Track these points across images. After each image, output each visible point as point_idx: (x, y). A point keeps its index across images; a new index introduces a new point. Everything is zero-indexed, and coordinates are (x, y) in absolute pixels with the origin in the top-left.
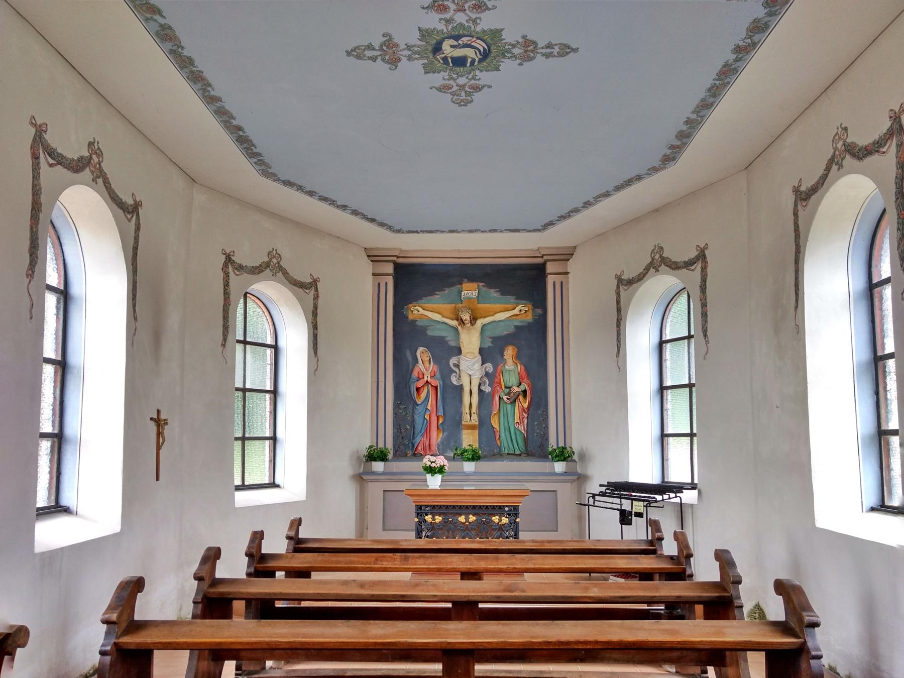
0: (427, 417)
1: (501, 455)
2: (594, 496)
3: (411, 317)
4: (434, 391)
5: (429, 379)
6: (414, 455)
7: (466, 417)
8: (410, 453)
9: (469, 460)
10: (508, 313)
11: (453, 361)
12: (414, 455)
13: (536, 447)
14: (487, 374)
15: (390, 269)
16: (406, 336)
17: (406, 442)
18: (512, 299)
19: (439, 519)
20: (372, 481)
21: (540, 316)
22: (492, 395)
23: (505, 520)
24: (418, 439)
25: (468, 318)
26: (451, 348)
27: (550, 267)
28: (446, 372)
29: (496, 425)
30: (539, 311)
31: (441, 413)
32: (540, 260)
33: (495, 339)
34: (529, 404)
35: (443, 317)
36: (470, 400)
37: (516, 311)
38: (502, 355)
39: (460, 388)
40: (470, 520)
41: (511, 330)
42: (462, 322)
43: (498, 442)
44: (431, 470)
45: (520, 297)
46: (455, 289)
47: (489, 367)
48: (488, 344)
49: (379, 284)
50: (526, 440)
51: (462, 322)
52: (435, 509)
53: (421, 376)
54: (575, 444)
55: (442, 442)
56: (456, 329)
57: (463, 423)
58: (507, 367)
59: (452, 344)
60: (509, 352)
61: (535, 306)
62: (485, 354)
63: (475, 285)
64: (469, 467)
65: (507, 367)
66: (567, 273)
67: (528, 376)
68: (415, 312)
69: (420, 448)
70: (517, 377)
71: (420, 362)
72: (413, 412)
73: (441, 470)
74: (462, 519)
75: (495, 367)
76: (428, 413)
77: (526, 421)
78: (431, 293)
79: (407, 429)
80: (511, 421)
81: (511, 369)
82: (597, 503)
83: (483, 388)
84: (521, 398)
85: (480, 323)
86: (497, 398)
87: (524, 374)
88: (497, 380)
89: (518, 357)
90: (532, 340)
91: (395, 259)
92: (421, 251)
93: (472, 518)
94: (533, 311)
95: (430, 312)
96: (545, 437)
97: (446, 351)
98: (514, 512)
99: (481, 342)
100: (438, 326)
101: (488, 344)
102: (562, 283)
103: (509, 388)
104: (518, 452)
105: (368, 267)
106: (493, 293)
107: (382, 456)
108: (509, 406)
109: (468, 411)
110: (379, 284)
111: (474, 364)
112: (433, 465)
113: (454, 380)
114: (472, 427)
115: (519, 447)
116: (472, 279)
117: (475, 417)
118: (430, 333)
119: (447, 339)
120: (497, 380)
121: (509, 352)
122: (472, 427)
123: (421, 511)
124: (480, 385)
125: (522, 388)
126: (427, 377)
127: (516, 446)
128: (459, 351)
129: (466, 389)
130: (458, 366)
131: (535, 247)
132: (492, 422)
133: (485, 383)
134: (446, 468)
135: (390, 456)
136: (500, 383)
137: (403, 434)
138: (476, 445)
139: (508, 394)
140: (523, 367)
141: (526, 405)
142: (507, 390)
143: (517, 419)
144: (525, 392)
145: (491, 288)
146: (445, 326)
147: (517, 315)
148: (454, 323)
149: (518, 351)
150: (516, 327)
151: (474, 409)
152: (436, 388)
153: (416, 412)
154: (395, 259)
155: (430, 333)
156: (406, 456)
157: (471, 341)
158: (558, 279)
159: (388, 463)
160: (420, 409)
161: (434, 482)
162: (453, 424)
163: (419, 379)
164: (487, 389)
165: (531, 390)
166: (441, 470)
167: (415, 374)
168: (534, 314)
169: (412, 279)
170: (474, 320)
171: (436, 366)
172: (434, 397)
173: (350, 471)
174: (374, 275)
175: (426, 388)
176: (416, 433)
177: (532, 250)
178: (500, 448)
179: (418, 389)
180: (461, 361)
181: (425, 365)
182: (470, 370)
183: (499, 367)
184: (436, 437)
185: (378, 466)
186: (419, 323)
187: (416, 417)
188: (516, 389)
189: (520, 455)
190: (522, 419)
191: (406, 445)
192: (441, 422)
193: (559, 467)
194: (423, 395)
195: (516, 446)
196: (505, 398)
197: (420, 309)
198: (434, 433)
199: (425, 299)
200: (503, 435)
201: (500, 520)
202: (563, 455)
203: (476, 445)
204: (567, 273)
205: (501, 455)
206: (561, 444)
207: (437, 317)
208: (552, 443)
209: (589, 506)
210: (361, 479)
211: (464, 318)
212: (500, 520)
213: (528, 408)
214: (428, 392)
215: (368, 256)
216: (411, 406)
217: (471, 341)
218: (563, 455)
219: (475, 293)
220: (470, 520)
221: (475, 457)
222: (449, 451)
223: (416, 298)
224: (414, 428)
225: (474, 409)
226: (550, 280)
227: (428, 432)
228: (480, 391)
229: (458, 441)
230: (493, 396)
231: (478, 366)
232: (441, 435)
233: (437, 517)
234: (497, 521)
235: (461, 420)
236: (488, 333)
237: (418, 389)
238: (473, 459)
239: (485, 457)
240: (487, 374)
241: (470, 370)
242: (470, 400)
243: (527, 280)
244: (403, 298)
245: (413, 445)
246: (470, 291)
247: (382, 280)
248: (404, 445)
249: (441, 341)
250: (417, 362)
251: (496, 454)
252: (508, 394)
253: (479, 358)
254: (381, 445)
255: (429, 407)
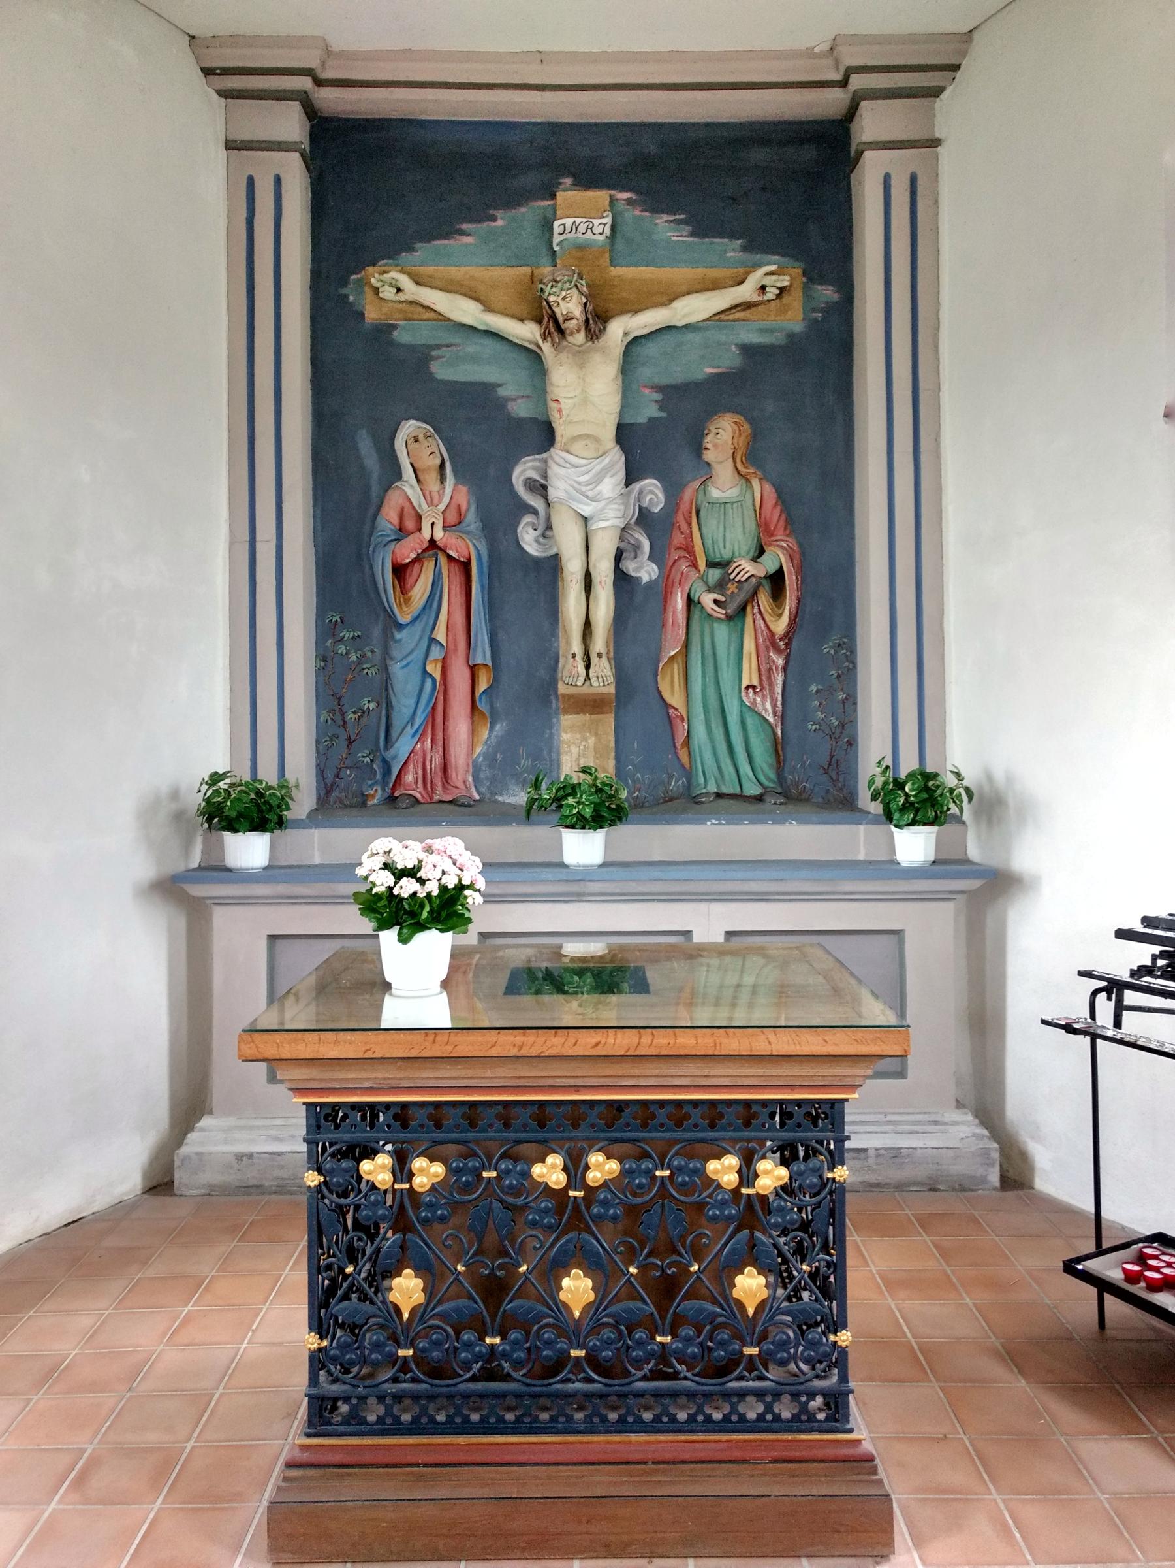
0: (434, 670)
1: (695, 800)
2: (1114, 987)
3: (372, 314)
4: (458, 579)
5: (439, 534)
6: (392, 800)
7: (571, 673)
8: (377, 795)
9: (580, 823)
10: (715, 298)
11: (524, 471)
12: (392, 800)
13: (812, 772)
14: (644, 518)
15: (290, 124)
16: (359, 380)
17: (363, 756)
18: (731, 248)
19: (427, 1173)
20: (223, 902)
21: (829, 309)
22: (663, 589)
23: (771, 1175)
24: (403, 747)
25: (577, 311)
26: (520, 423)
27: (873, 123)
28: (501, 511)
29: (675, 698)
30: (827, 293)
31: (482, 655)
32: (831, 102)
33: (671, 393)
34: (793, 621)
35: (488, 308)
36: (586, 610)
37: (746, 292)
38: (698, 449)
39: (552, 566)
40: (594, 1177)
41: (730, 360)
42: (555, 327)
43: (683, 754)
44: (400, 914)
45: (758, 244)
46: (530, 212)
47: (652, 492)
48: (648, 410)
49: (251, 181)
50: (778, 748)
51: (555, 327)
52: (410, 1127)
53: (410, 524)
54: (961, 756)
55: (491, 759)
56: (534, 356)
57: (562, 689)
58: (715, 493)
59: (521, 409)
60: (724, 435)
61: (812, 277)
62: (640, 449)
63: (601, 196)
64: (583, 848)
65: (715, 493)
66: (934, 143)
67: (791, 523)
68: (388, 293)
69: (409, 778)
70: (751, 525)
71: (408, 473)
72: (386, 653)
73: (447, 909)
74: (550, 1171)
75: (673, 491)
76: (436, 653)
77: (779, 680)
78: (446, 229)
79: (364, 713)
80: (731, 685)
81: (730, 498)
82: (1133, 1023)
83: (629, 566)
84: (764, 599)
85: (618, 330)
86: (680, 603)
87: (774, 515)
88: (678, 539)
89: (751, 457)
90: (800, 401)
91: (305, 83)
92: (407, 54)
93: (602, 1168)
94: (806, 289)
95: (438, 293)
96: (844, 737)
97: (501, 436)
98: (808, 1130)
99: (624, 407)
100: (472, 347)
101: (648, 410)
102: (913, 180)
103: (723, 565)
104: (752, 790)
105: (203, 117)
106: (666, 229)
107: (255, 809)
108: (722, 632)
109: (577, 647)
110: (251, 181)
111: (598, 480)
112: (407, 887)
113: (529, 540)
114: (591, 705)
115: (755, 770)
116: (590, 177)
117: (603, 669)
118: (441, 371)
119: (502, 392)
120: (678, 539)
121: (724, 435)
122: (591, 705)
123: (341, 1133)
124: (619, 556)
125: (769, 564)
126: (432, 528)
127: (745, 769)
128: (544, 435)
129: (573, 568)
130: (540, 489)
131: (819, 40)
132: (664, 687)
133: (637, 548)
134: (473, 898)
135: (303, 803)
136: (689, 549)
137: (353, 731)
138: (607, 769)
139: (720, 586)
140: (768, 488)
141: (780, 626)
142: (715, 575)
143: (750, 676)
144: (776, 580)
145: (656, 210)
146: (491, 345)
147: (747, 306)
148: (526, 332)
149: (755, 435)
150: (748, 350)
151: (599, 643)
152: (466, 566)
153: (396, 653)
154: (305, 83)
155: (441, 371)
156: (364, 804)
157: (587, 394)
158: (898, 163)
159: (289, 836)
160: (407, 639)
161: (417, 979)
162: (525, 691)
163: (402, 532)
164: (645, 571)
165: (800, 570)
166: (447, 909)
167: (389, 517)
168: (809, 308)
169: (374, 173)
170: (596, 321)
171: (463, 489)
172: (458, 590)
173: (143, 868)
174: (230, 145)
175: (429, 566)
176: (397, 723)
177: (810, 53)
178: (689, 774)
179: (400, 571)
180: (554, 470)
181: (425, 491)
182: (585, 498)
183: (688, 494)
184: (467, 742)
185: (249, 850)
186: (402, 336)
187: (396, 669)
188: (747, 568)
189: (760, 799)
190: (765, 674)
191: (363, 775)
192: (483, 686)
193: (914, 845)
194: (420, 590)
195: (745, 769)
196: (708, 600)
197: (405, 281)
198: (460, 726)
199: (423, 250)
200: (700, 732)
201: (747, 1175)
202: (922, 799)
203: (607, 769)
204: (934, 143)
205: (695, 800)
206: (908, 764)
207: (465, 311)
208: (873, 753)
209: (1094, 1037)
210: (187, 896)
211: (561, 311)
212: (747, 1175)
213: (788, 636)
214: (436, 582)
215: (207, 72)
216: (377, 632)
217: (587, 394)
218: (922, 799)
219: (601, 226)
220: (594, 1177)
221: (604, 813)
222: (514, 787)
223: (393, 248)
224: (389, 705)
225: (599, 643)
226: (872, 171)
227: (437, 720)
228: (622, 579)
229: (547, 753)
230: (666, 596)
231: (611, 485)
232: (484, 733)
233: (419, 1163)
234: (730, 1179)
235: (553, 682)
236: (646, 373)
237: (400, 571)
238: (596, 821)
239: (639, 805)
240: (644, 518)
241: (585, 498)
242: (586, 610)
243: (784, 177)
244: (348, 234)
245: (387, 766)
246: (583, 217)
247: (265, 166)
248: (356, 766)
249: (480, 399)
250: (399, 475)
251: (681, 800)
252: (720, 586)
253: (616, 457)
254: (268, 775)
255: (441, 635)
